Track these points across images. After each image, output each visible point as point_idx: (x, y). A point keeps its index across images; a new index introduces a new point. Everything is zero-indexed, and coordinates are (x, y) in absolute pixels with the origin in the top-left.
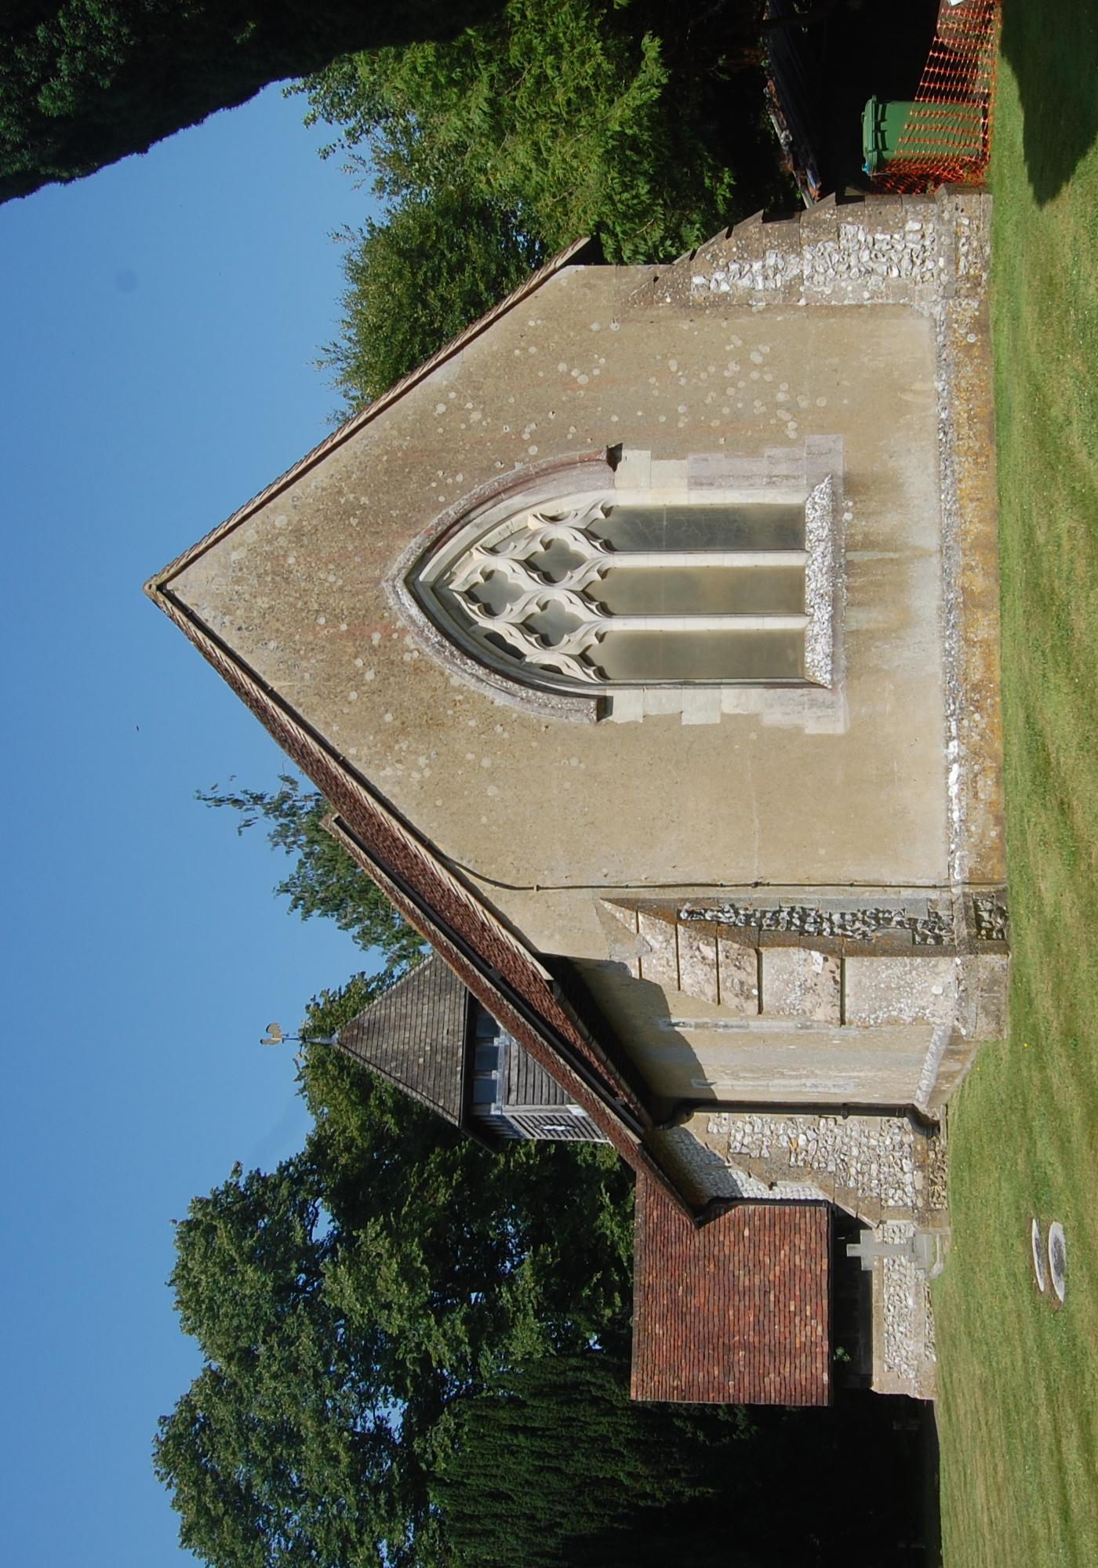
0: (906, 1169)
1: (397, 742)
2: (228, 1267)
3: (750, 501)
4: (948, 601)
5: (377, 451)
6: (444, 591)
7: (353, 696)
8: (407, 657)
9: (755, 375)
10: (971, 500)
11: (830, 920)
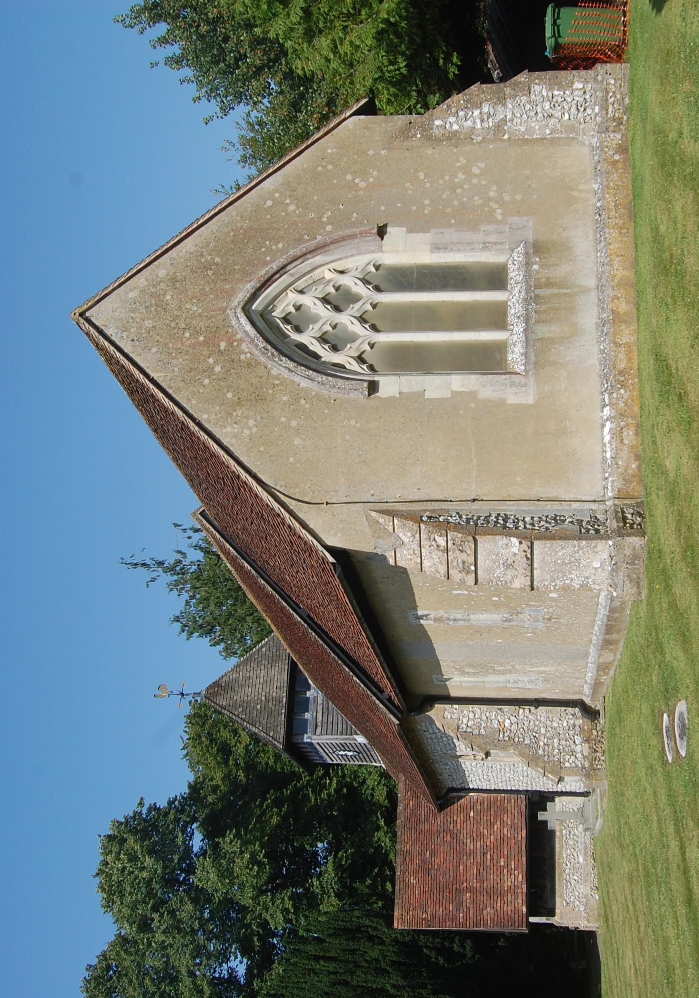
0: (577, 742)
1: (235, 410)
2: (133, 858)
3: (471, 260)
4: (602, 319)
5: (226, 230)
6: (268, 317)
7: (206, 381)
8: (243, 357)
9: (475, 181)
10: (618, 256)
11: (523, 520)
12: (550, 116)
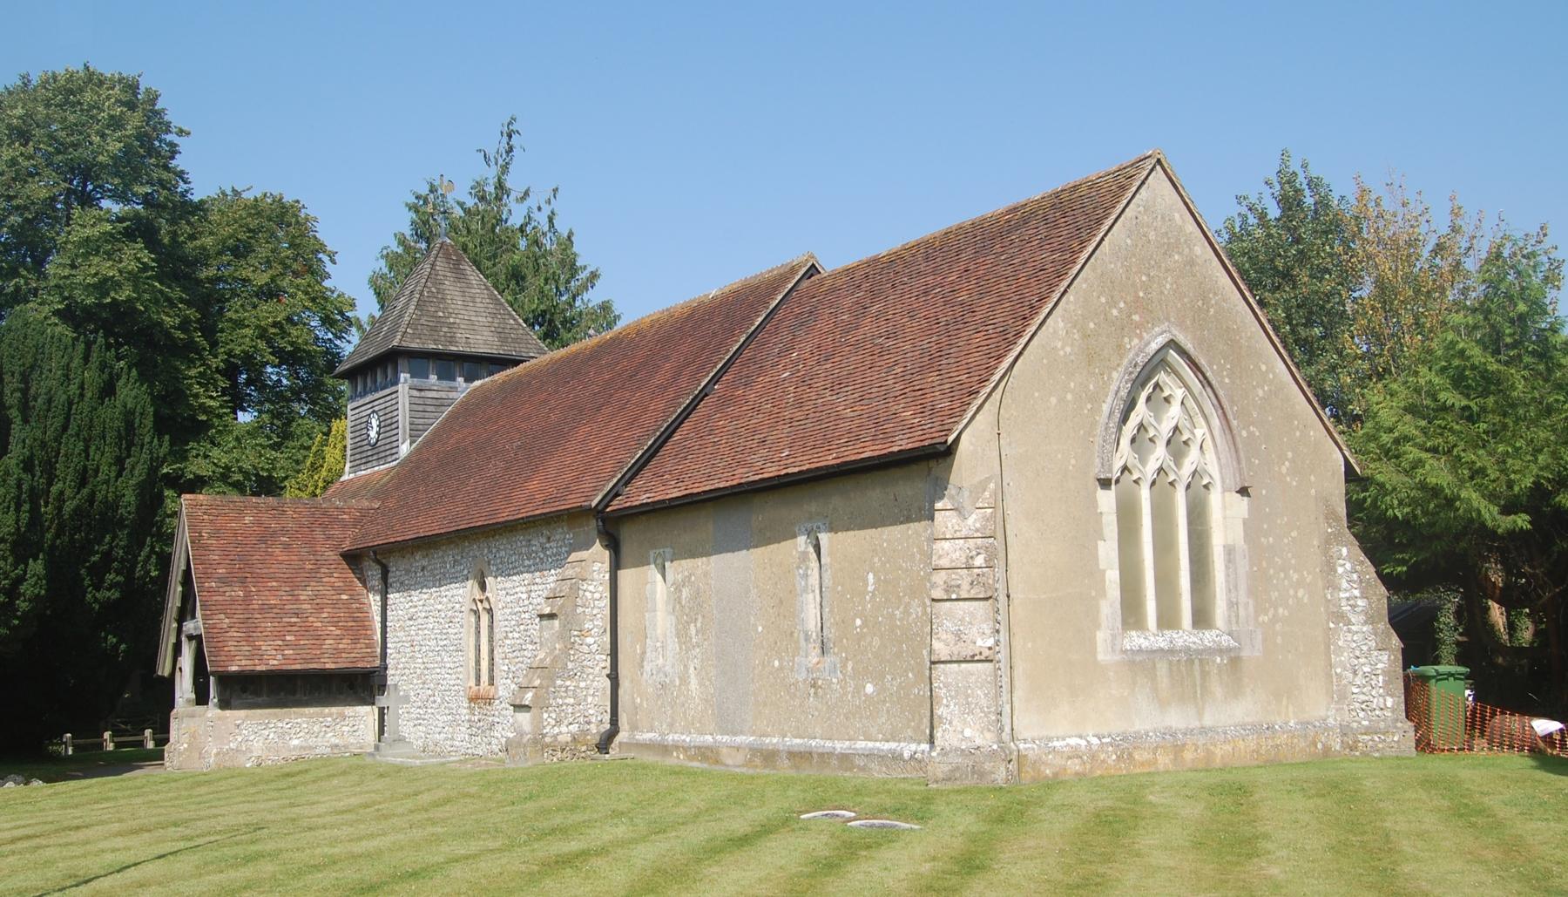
2: (116, 123)
7: (1103, 300)
9: (1292, 592)
12: (1355, 673)
